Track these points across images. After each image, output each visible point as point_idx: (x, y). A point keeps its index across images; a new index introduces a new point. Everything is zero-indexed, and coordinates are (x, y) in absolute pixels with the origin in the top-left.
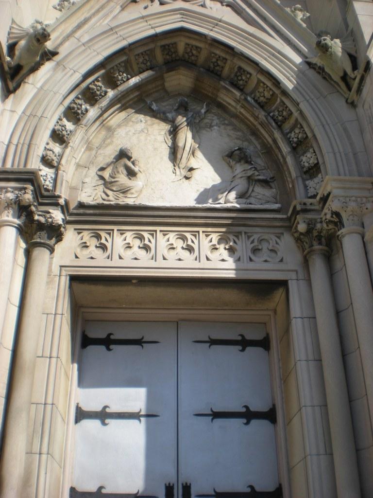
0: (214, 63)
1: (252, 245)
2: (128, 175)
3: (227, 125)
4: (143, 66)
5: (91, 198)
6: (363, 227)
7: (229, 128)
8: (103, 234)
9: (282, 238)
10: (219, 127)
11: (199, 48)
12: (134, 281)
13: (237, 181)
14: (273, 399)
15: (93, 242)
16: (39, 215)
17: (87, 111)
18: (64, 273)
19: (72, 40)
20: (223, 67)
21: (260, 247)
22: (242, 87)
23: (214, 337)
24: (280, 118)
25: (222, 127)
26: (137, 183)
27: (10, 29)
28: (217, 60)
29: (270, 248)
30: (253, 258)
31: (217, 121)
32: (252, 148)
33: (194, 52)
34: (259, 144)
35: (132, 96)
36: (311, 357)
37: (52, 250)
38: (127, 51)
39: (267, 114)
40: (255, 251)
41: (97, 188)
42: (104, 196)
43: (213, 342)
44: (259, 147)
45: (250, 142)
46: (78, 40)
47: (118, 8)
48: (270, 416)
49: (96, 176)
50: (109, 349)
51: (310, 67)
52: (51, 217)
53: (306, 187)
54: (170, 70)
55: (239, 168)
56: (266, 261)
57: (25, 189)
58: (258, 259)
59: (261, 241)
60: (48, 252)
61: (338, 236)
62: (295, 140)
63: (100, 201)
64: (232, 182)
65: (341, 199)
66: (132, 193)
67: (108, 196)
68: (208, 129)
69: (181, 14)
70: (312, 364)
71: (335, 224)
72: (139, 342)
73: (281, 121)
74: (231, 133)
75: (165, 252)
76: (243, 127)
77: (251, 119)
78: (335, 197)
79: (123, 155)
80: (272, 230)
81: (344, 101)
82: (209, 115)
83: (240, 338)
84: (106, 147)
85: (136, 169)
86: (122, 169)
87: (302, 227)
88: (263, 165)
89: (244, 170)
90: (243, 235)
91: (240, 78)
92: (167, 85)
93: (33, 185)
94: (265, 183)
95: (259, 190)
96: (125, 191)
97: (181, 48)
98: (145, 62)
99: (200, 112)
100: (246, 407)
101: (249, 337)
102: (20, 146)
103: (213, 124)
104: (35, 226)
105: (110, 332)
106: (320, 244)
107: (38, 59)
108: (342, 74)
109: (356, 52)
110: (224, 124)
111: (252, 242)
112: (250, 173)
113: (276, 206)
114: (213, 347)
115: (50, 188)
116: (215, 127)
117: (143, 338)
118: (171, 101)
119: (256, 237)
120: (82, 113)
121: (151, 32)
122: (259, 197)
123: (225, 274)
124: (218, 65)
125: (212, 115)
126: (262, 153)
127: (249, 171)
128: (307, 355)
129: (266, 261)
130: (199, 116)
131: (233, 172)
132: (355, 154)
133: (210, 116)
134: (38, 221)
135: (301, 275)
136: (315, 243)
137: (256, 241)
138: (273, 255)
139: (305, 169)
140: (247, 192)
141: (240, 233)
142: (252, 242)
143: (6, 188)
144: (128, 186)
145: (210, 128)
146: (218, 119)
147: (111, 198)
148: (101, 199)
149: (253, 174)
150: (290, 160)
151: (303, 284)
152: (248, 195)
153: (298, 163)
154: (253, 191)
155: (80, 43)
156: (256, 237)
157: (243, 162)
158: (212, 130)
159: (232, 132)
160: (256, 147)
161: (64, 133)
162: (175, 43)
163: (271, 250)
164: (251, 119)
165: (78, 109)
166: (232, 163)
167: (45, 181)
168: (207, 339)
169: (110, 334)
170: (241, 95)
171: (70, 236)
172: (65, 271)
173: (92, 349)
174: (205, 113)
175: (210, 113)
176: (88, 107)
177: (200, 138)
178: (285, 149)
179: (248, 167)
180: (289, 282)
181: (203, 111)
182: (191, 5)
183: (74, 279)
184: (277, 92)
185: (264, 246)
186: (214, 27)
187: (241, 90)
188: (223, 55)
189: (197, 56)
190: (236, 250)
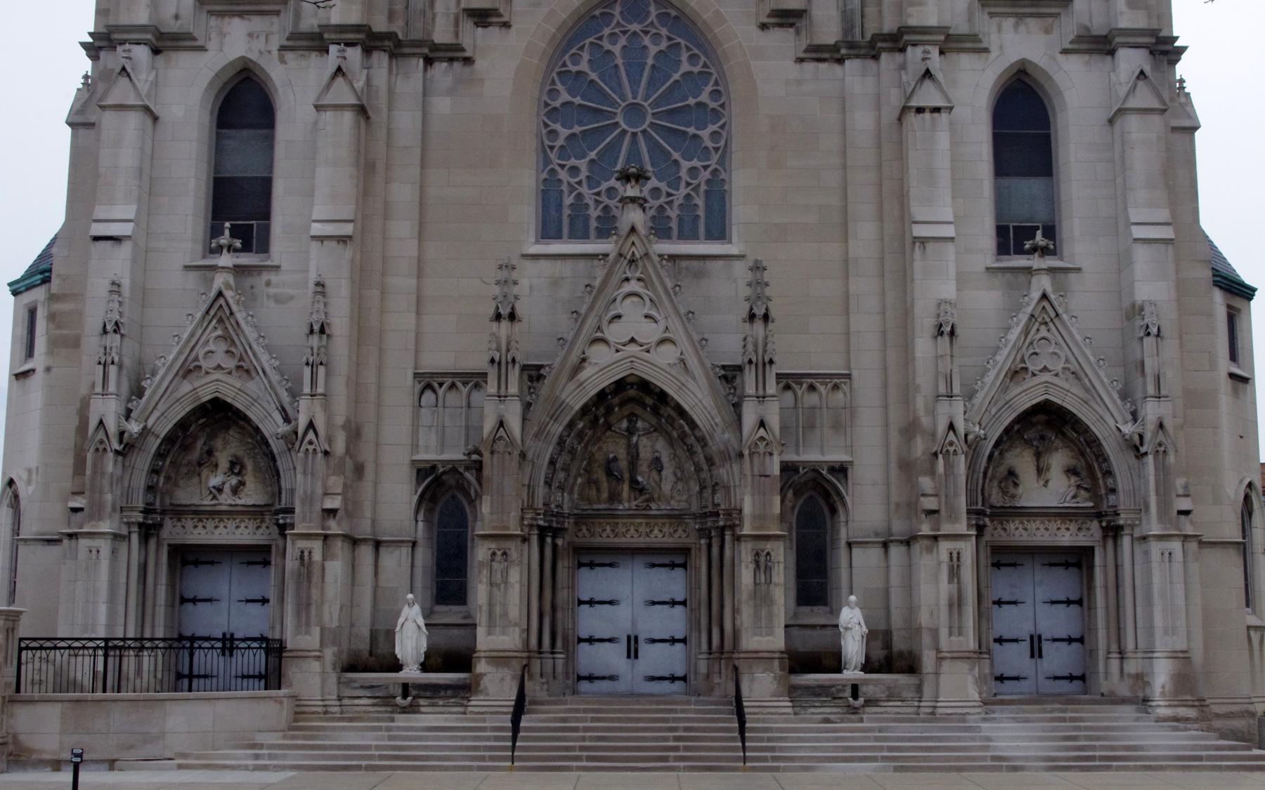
15: (999, 527)
26: (1020, 490)
32: (1080, 464)
40: (1079, 529)
43: (1051, 565)
48: (1081, 640)
55: (1073, 479)
58: (1081, 535)
86: (1010, 482)
87: (1104, 524)
94: (1086, 489)
96: (1013, 497)
101: (1070, 561)
107: (1016, 428)
113: (1091, 504)
150: (1101, 482)
153: (1105, 483)
170: (848, 604)
171: (168, 523)
178: (1100, 475)
183: (169, 545)
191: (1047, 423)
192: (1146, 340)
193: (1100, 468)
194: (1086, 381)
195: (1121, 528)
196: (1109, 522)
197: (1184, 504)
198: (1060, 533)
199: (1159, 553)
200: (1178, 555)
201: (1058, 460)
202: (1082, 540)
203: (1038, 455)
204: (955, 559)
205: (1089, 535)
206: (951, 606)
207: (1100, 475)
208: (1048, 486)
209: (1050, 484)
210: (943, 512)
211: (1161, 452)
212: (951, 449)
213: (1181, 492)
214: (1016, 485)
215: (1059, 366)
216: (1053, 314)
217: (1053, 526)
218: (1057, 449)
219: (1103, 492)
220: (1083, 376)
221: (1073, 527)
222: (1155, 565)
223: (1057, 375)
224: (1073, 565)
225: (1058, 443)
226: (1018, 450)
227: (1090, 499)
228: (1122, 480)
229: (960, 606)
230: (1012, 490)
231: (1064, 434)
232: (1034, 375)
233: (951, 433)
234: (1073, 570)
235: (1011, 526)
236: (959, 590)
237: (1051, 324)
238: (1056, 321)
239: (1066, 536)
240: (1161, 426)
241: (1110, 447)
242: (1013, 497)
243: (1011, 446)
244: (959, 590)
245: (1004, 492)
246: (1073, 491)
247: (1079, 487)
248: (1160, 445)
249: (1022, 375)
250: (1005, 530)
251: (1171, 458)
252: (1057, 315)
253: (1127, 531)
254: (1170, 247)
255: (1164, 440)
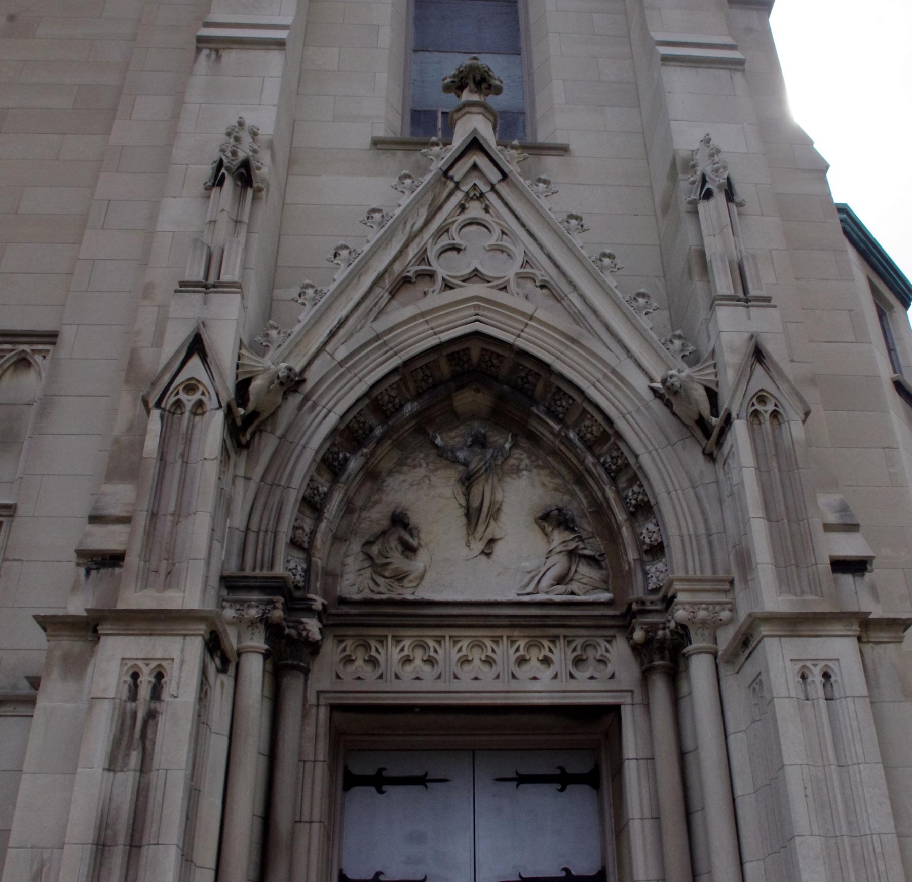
0: (523, 378)
1: (575, 654)
2: (403, 553)
3: (542, 468)
4: (423, 384)
5: (355, 589)
6: (716, 643)
7: (544, 472)
8: (373, 643)
9: (614, 643)
10: (530, 471)
11: (502, 356)
12: (417, 709)
13: (555, 558)
14: (604, 858)
15: (360, 656)
16: (289, 627)
17: (346, 460)
18: (322, 701)
19: (324, 357)
20: (535, 386)
21: (584, 657)
22: (561, 416)
23: (523, 772)
24: (613, 467)
25: (534, 471)
26: (419, 563)
27: (239, 359)
28: (527, 375)
29: (598, 657)
30: (574, 672)
31: (528, 461)
32: (576, 504)
33: (495, 361)
34: (586, 497)
35: (407, 427)
36: (647, 814)
37: (306, 672)
38: (401, 369)
39: (596, 461)
40: (578, 662)
41: (362, 572)
42: (372, 585)
43: (522, 780)
44: (584, 501)
45: (573, 495)
46: (332, 355)
47: (387, 296)
49: (361, 554)
50: (381, 792)
51: (656, 397)
52: (305, 629)
53: (645, 573)
54: (460, 387)
55: (558, 537)
56: (592, 678)
57: (272, 602)
58: (582, 674)
59: (585, 647)
60: (302, 676)
61: (684, 655)
62: (633, 502)
63: (367, 594)
64: (547, 558)
65: (687, 607)
66: (411, 581)
67: (377, 584)
68: (514, 476)
69: (605, 376)
70: (648, 823)
71: (682, 636)
72: (421, 781)
73: (613, 472)
74: (547, 480)
75: (456, 669)
76: (564, 471)
77: (575, 461)
78: (683, 603)
79: (399, 520)
80: (600, 632)
81: (700, 450)
82: (516, 451)
83: (558, 772)
84: (373, 507)
85: (414, 542)
86: (393, 543)
87: (639, 635)
88: (590, 530)
89: (564, 542)
90: (562, 640)
91: (559, 403)
92: (455, 404)
93: (283, 596)
94: (592, 561)
95: (584, 570)
96: (400, 577)
97: (475, 354)
98: (425, 378)
99: (503, 447)
100: (566, 870)
102: (262, 534)
103: (522, 466)
104: (284, 641)
105: (381, 766)
106: (662, 658)
108: (696, 417)
109: (717, 385)
110: (537, 466)
111: (574, 650)
112: (572, 545)
113: (605, 596)
114: (522, 786)
115: (301, 584)
116: (525, 472)
117: (426, 774)
118: (462, 430)
119: (579, 642)
120: (339, 464)
121: (433, 341)
122: (583, 581)
123: (538, 698)
124: (528, 382)
125: (520, 451)
126: (589, 513)
127: (571, 543)
128: (642, 811)
129: (592, 678)
130: (502, 456)
131: (549, 542)
132: (709, 535)
133: (517, 453)
134: (289, 635)
135: (638, 698)
136: (656, 657)
137: (579, 648)
138: (602, 667)
139: (645, 547)
140: (567, 574)
141: (558, 637)
142: (574, 650)
143: (251, 601)
144: (405, 569)
145: (516, 473)
146: (529, 458)
147: (382, 589)
148: (368, 590)
149: (577, 547)
150: (625, 532)
151: (639, 710)
152: (569, 578)
153: (637, 536)
154: (576, 571)
155: (335, 363)
156: (579, 642)
157: (562, 528)
158: (519, 477)
159: (548, 478)
160: (580, 503)
161: (317, 498)
162: (468, 349)
163: (600, 661)
164: (575, 461)
165: (334, 459)
166: (549, 529)
167: (294, 575)
168: (515, 775)
169: (381, 770)
171: (331, 651)
172: (325, 698)
173: (356, 791)
174: (510, 449)
175: (517, 448)
176: (348, 455)
177: (503, 490)
179: (568, 536)
180: (622, 707)
181: (507, 446)
182: (489, 289)
183: (334, 708)
184: (610, 431)
185: (591, 654)
186: (522, 331)
187: (560, 421)
188: (535, 369)
189: (498, 367)
190: (552, 662)
191: (482, 396)
192: (702, 207)
193: (623, 500)
194: (574, 298)
195: (682, 633)
196: (651, 629)
197: (850, 547)
198: (524, 672)
199: (793, 671)
200: (850, 674)
201: (521, 494)
202: (586, 688)
203: (468, 481)
204: (145, 691)
205: (606, 674)
206: (101, 847)
207: (621, 516)
208: (487, 545)
209: (499, 549)
210: (133, 560)
211: (765, 413)
212: (189, 400)
213: (832, 518)
214: (410, 550)
215: (511, 270)
216: (495, 176)
217: (505, 653)
218: (517, 470)
219: (632, 555)
220: (565, 288)
221: (561, 655)
222: (785, 709)
223: (504, 288)
224: (578, 779)
225: (520, 457)
226: (421, 471)
227: (605, 585)
228: (676, 519)
229: (135, 844)
230: (397, 560)
231: (534, 438)
232: (448, 286)
233: (195, 360)
234: (579, 794)
235: (391, 654)
236: (142, 794)
237: (492, 197)
238: (502, 188)
239: (543, 679)
240: (758, 354)
241: (643, 431)
242: (400, 577)
243: (401, 463)
244: (142, 794)
245: (377, 566)
246: (559, 564)
247: (572, 554)
248: (762, 399)
249: (422, 286)
250: (373, 662)
251: (796, 429)
252: (504, 176)
253: (698, 641)
254: (738, 76)
255: (770, 387)
